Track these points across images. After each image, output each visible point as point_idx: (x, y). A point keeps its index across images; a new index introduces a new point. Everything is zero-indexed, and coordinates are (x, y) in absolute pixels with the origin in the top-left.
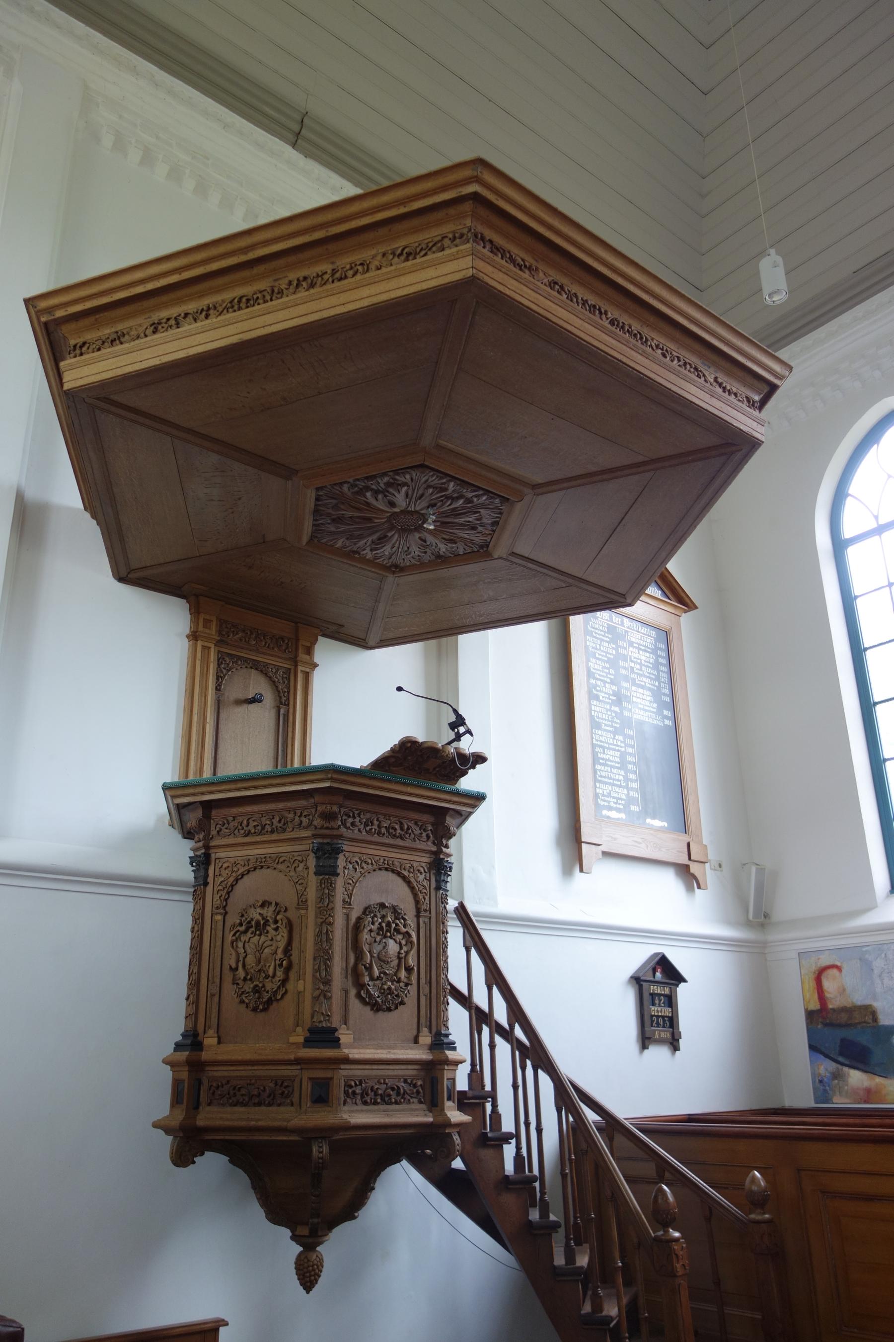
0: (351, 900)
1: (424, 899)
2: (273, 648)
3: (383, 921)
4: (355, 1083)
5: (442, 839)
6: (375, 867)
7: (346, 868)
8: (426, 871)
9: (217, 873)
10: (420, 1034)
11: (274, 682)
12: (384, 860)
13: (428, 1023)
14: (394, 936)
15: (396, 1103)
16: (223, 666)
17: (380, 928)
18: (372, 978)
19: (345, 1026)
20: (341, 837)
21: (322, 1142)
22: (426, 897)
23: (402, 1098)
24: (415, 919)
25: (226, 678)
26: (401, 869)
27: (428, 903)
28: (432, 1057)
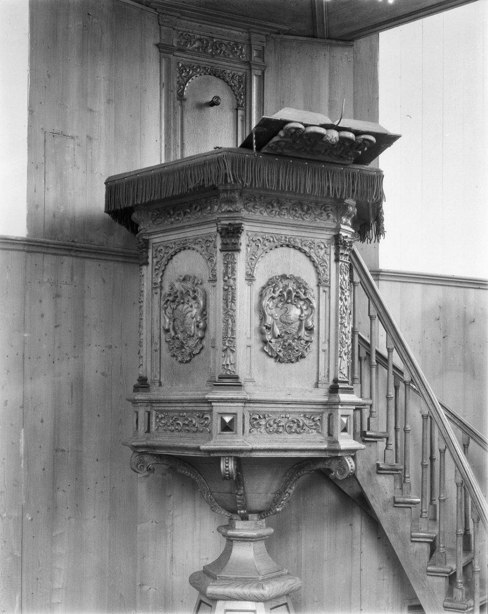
0: (253, 273)
1: (324, 270)
2: (228, 55)
3: (285, 290)
4: (259, 417)
6: (277, 243)
7: (248, 246)
9: (154, 256)
11: (231, 86)
12: (286, 238)
15: (296, 432)
16: (183, 74)
17: (281, 295)
18: (274, 337)
20: (243, 219)
21: (228, 460)
22: (326, 270)
23: (302, 429)
25: (187, 85)
26: (302, 246)
28: (327, 399)
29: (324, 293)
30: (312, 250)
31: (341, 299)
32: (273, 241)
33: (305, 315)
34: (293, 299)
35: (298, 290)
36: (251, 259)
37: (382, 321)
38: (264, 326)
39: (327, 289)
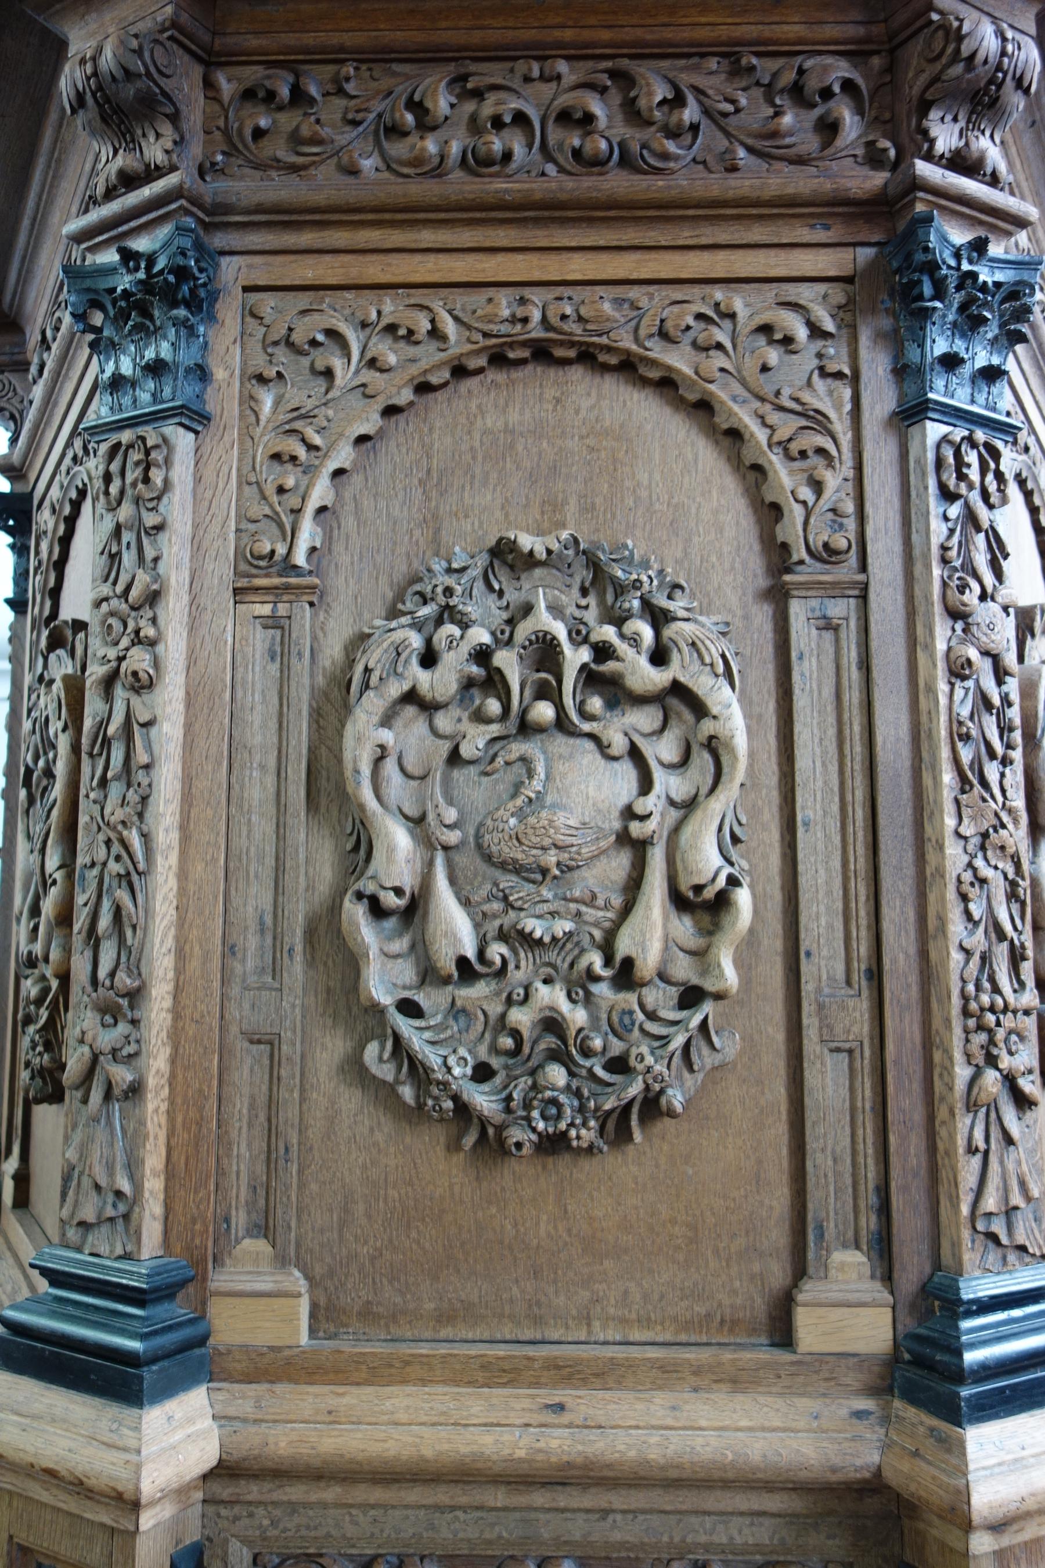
5: (924, 107)
8: (829, 326)
10: (808, 1291)
13: (870, 1222)
14: (586, 716)
19: (262, 1246)
24: (763, 616)
26: (637, 340)
27: (850, 507)
29: (828, 636)
30: (719, 360)
31: (959, 671)
32: (435, 333)
33: (672, 803)
34: (568, 701)
35: (609, 633)
36: (276, 457)
37: (857, 748)
38: (359, 896)
39: (840, 609)
